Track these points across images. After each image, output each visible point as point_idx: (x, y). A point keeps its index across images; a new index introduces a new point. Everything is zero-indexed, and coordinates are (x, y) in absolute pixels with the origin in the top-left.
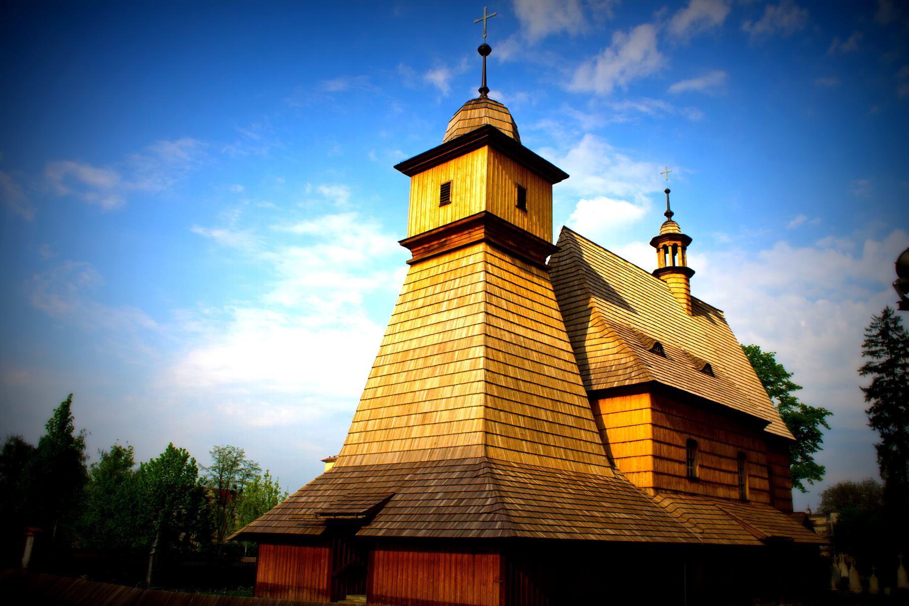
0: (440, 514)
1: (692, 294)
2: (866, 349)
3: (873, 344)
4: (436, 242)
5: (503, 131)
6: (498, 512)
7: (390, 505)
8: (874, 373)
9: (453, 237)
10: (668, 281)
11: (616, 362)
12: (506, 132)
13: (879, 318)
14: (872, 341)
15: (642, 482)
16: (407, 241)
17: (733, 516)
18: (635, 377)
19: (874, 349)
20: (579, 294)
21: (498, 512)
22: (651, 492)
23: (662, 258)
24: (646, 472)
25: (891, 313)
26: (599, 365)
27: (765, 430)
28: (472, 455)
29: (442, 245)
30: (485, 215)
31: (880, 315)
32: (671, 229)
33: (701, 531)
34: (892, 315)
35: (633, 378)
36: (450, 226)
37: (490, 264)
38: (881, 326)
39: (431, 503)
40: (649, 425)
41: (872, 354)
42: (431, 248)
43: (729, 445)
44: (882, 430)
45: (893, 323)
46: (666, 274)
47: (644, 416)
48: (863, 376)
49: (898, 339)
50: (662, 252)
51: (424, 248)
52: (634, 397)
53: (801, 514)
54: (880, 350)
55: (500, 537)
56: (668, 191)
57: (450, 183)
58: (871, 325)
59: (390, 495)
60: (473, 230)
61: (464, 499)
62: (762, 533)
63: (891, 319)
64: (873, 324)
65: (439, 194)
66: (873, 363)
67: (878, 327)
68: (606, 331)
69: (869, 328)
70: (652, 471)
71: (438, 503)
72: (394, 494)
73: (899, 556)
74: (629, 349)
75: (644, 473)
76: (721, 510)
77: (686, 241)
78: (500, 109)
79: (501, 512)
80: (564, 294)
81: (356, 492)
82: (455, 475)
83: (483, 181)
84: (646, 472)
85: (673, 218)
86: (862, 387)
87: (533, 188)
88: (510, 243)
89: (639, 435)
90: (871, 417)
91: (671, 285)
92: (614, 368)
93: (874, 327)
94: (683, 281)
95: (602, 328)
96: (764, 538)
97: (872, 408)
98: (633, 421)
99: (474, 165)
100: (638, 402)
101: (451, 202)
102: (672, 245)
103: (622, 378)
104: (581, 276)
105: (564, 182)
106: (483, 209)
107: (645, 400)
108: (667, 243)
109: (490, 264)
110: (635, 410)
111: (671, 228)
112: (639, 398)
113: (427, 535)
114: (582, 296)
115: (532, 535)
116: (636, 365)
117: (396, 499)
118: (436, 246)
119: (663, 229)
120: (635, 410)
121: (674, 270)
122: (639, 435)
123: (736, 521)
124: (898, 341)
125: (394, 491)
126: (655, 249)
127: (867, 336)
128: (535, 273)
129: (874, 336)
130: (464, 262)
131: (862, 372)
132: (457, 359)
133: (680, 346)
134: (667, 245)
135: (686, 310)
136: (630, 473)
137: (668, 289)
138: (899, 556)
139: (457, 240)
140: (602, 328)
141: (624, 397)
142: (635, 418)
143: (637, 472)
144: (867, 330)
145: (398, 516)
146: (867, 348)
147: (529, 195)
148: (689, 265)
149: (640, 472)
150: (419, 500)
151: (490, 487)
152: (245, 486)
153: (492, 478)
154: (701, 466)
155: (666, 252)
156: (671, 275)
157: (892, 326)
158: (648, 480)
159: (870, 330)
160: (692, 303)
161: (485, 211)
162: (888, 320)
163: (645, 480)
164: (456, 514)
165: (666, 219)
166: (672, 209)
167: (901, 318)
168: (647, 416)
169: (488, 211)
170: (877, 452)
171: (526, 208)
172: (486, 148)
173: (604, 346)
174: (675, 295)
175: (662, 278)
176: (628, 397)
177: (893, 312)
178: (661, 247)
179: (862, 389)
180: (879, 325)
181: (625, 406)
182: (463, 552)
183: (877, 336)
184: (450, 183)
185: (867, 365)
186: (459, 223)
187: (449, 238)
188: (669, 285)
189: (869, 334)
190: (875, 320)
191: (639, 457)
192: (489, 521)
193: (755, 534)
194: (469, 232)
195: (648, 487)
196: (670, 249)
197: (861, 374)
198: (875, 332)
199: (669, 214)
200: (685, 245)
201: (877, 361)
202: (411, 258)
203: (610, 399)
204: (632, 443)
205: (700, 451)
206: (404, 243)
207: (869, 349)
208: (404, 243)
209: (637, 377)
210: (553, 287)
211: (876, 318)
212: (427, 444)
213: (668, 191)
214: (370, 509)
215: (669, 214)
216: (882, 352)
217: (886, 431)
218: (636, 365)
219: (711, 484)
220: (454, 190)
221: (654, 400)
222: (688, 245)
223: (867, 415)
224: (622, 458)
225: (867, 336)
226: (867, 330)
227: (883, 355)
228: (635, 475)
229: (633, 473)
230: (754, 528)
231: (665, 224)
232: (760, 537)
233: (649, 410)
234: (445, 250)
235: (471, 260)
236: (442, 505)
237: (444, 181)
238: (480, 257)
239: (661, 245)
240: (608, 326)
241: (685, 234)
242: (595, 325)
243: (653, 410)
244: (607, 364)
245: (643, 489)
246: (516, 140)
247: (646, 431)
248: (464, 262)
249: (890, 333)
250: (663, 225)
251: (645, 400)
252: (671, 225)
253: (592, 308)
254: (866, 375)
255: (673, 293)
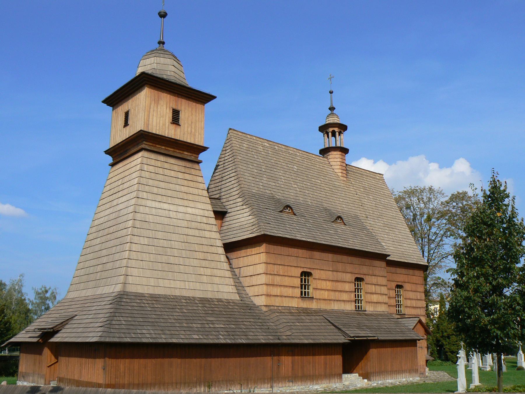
32: (332, 120)
65: (124, 117)
74: (256, 212)
77: (343, 128)
78: (167, 53)
85: (335, 112)
95: (243, 198)
111: (331, 119)
115: (183, 341)
119: (327, 120)
134: (336, 131)
140: (243, 198)
147: (170, 116)
152: (445, 327)
165: (330, 112)
199: (332, 109)
202: (112, 161)
206: (107, 152)
215: (332, 109)
234: (128, 155)
252: (332, 117)
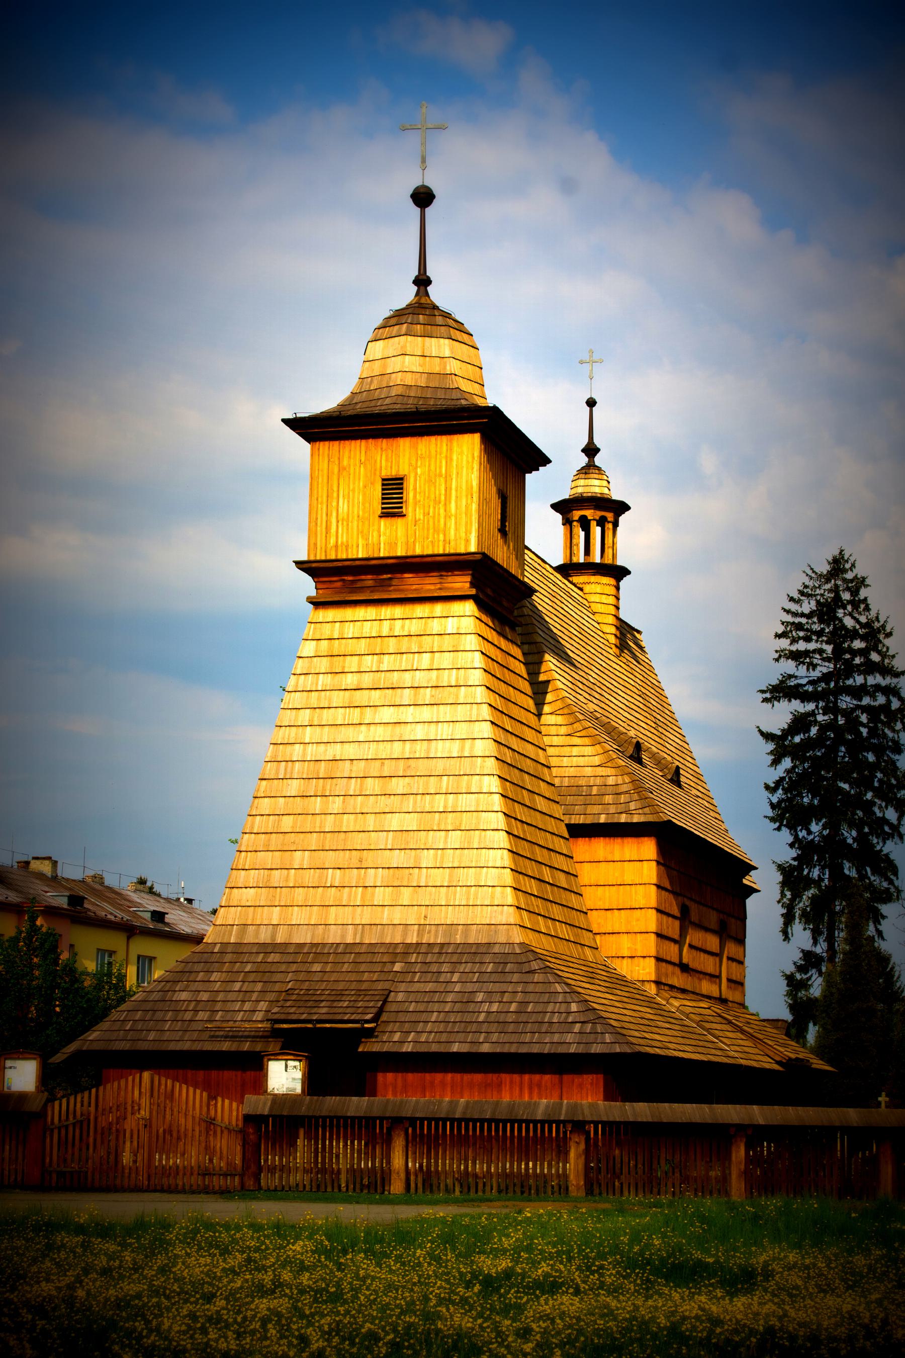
1: (622, 616)
2: (784, 643)
3: (801, 634)
4: (369, 577)
8: (793, 700)
9: (406, 575)
10: (587, 588)
11: (598, 781)
13: (821, 575)
14: (799, 627)
15: (639, 973)
16: (314, 565)
17: (737, 1026)
18: (637, 812)
19: (802, 646)
22: (652, 989)
24: (644, 957)
25: (848, 566)
26: (566, 782)
27: (745, 881)
29: (383, 585)
31: (824, 568)
32: (594, 487)
34: (850, 572)
35: (633, 812)
36: (408, 560)
38: (822, 595)
40: (652, 886)
41: (796, 656)
42: (359, 585)
43: (713, 909)
44: (796, 831)
45: (848, 589)
46: (582, 574)
47: (645, 871)
48: (770, 705)
49: (855, 631)
51: (344, 580)
52: (630, 840)
53: (780, 1023)
54: (814, 651)
55: (386, 1052)
56: (591, 403)
58: (801, 588)
60: (450, 574)
62: (781, 1052)
63: (845, 580)
64: (806, 587)
66: (796, 677)
67: (815, 595)
68: (577, 726)
69: (796, 595)
70: (654, 957)
73: (880, 1099)
75: (641, 959)
76: (720, 1016)
83: (472, 495)
84: (644, 957)
86: (764, 730)
89: (636, 900)
90: (775, 800)
91: (592, 598)
93: (808, 596)
96: (784, 1061)
97: (782, 779)
98: (625, 878)
99: (451, 460)
100: (636, 848)
101: (405, 515)
102: (597, 518)
103: (612, 809)
107: (648, 848)
108: (589, 513)
110: (629, 861)
111: (597, 482)
112: (639, 843)
114: (531, 656)
116: (636, 791)
118: (370, 583)
120: (629, 861)
122: (636, 900)
123: (742, 1034)
124: (853, 634)
127: (788, 612)
129: (803, 615)
130: (435, 626)
131: (768, 695)
132: (447, 788)
133: (629, 728)
134: (589, 518)
135: (613, 646)
136: (618, 957)
138: (880, 1099)
139: (413, 583)
141: (612, 838)
142: (630, 873)
143: (630, 957)
144: (792, 599)
146: (788, 641)
149: (634, 957)
154: (691, 946)
156: (593, 579)
157: (846, 596)
158: (647, 970)
159: (797, 601)
162: (839, 583)
163: (643, 970)
166: (597, 442)
167: (867, 582)
168: (650, 872)
170: (780, 878)
173: (575, 751)
174: (597, 617)
175: (575, 579)
176: (619, 840)
177: (853, 565)
178: (576, 518)
179: (762, 733)
180: (818, 591)
181: (612, 853)
182: (445, 1070)
183: (809, 616)
185: (782, 682)
186: (429, 559)
187: (399, 575)
188: (586, 596)
189: (793, 610)
190: (811, 578)
191: (634, 935)
193: (771, 1054)
194: (441, 576)
195: (648, 981)
197: (765, 700)
198: (808, 606)
201: (802, 674)
202: (313, 593)
203: (587, 839)
204: (622, 911)
207: (791, 644)
208: (302, 566)
210: (524, 654)
211: (813, 575)
212: (412, 916)
213: (591, 403)
216: (818, 656)
217: (802, 834)
218: (636, 791)
219: (697, 975)
220: (409, 494)
221: (662, 849)
223: (767, 794)
224: (605, 933)
225: (788, 612)
226: (792, 599)
227: (820, 662)
228: (625, 961)
229: (623, 957)
230: (770, 1046)
232: (778, 1058)
233: (654, 864)
235: (451, 625)
239: (577, 514)
240: (581, 717)
241: (627, 502)
242: (557, 712)
244: (582, 782)
247: (649, 896)
248: (435, 626)
249: (840, 613)
251: (648, 848)
253: (547, 682)
254: (776, 703)
255: (594, 613)
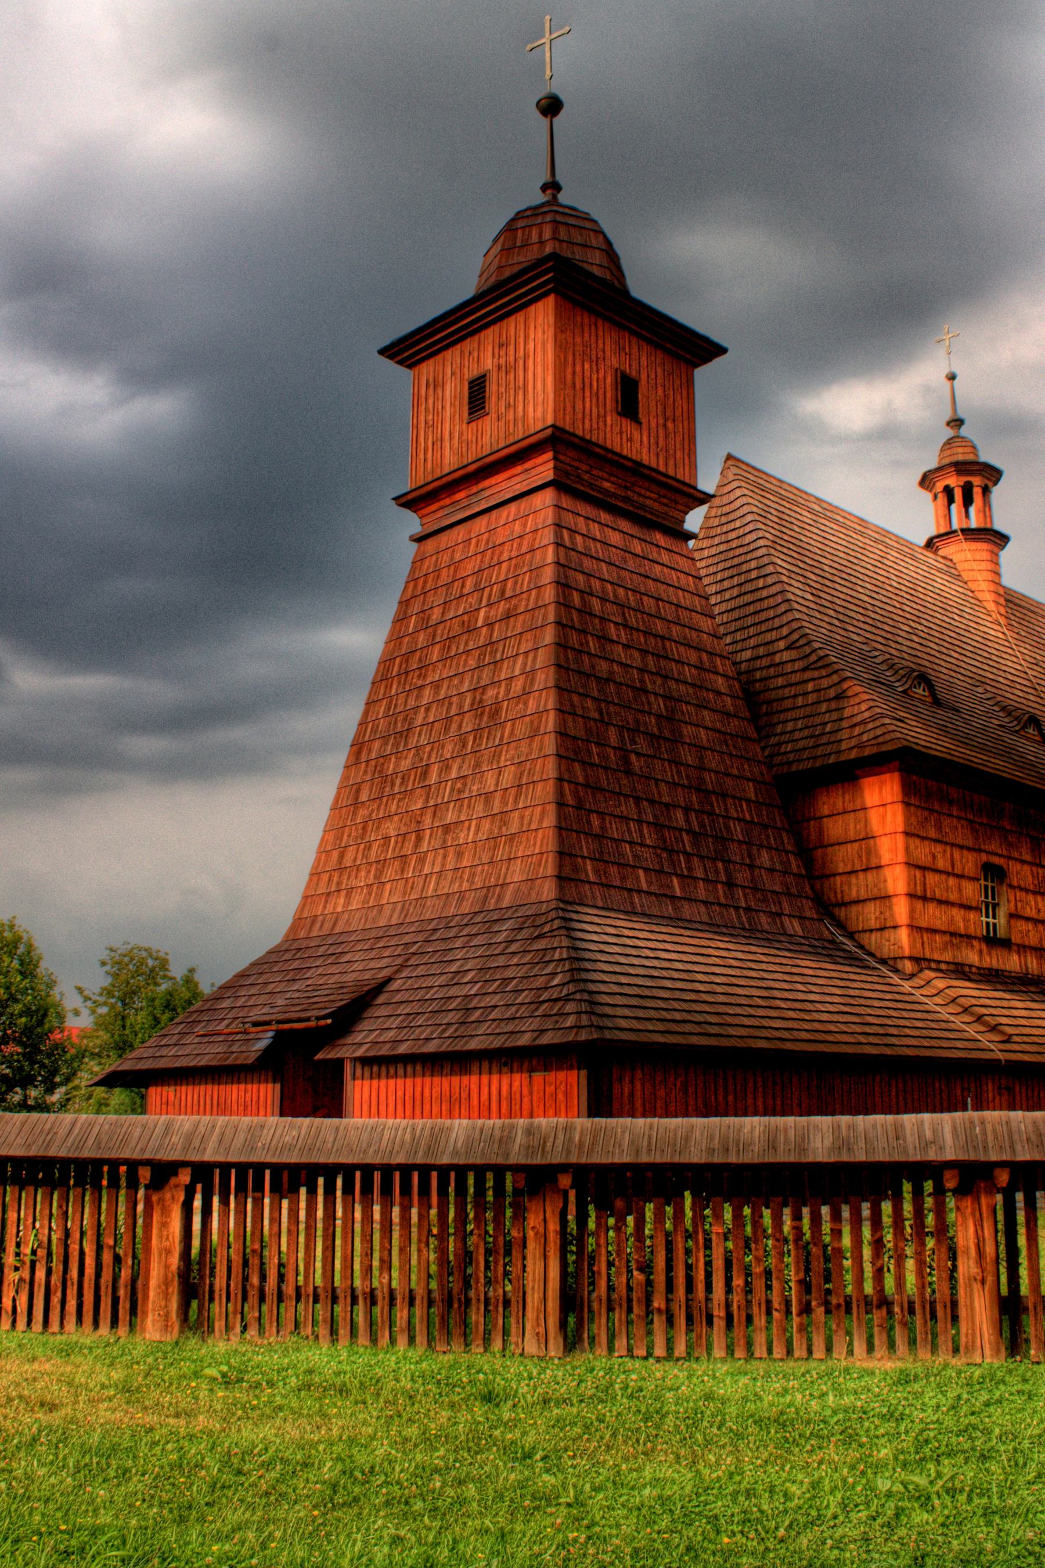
0: (468, 1009)
5: (586, 266)
6: (571, 997)
7: (381, 999)
12: (595, 267)
16: (410, 497)
20: (761, 585)
21: (571, 997)
23: (942, 511)
28: (533, 898)
30: (553, 434)
33: (1005, 1038)
37: (567, 528)
39: (453, 991)
50: (942, 499)
56: (952, 377)
57: (485, 376)
59: (380, 981)
61: (514, 978)
71: (465, 990)
72: (389, 980)
79: (578, 996)
80: (767, 609)
81: (321, 982)
82: (501, 937)
85: (964, 431)
87: (601, 333)
88: (607, 485)
92: (828, 728)
94: (986, 555)
102: (962, 484)
104: (764, 551)
105: (718, 362)
106: (550, 421)
109: (567, 528)
113: (443, 1049)
117: (392, 989)
121: (970, 534)
125: (388, 974)
126: (928, 496)
128: (663, 545)
134: (952, 486)
137: (956, 573)
145: (393, 1018)
148: (999, 525)
150: (431, 987)
151: (561, 953)
153: (568, 936)
155: (951, 500)
160: (1006, 600)
161: (553, 426)
164: (495, 1007)
165: (950, 433)
169: (558, 424)
171: (640, 416)
172: (551, 300)
184: (485, 376)
192: (555, 1015)
196: (958, 494)
200: (990, 484)
205: (1011, 886)
209: (874, 742)
214: (340, 1008)
220: (492, 388)
222: (996, 483)
229: (871, 931)
231: (949, 443)
236: (472, 992)
237: (475, 373)
238: (548, 516)
243: (907, 804)
245: (891, 962)
246: (616, 284)
250: (944, 444)
